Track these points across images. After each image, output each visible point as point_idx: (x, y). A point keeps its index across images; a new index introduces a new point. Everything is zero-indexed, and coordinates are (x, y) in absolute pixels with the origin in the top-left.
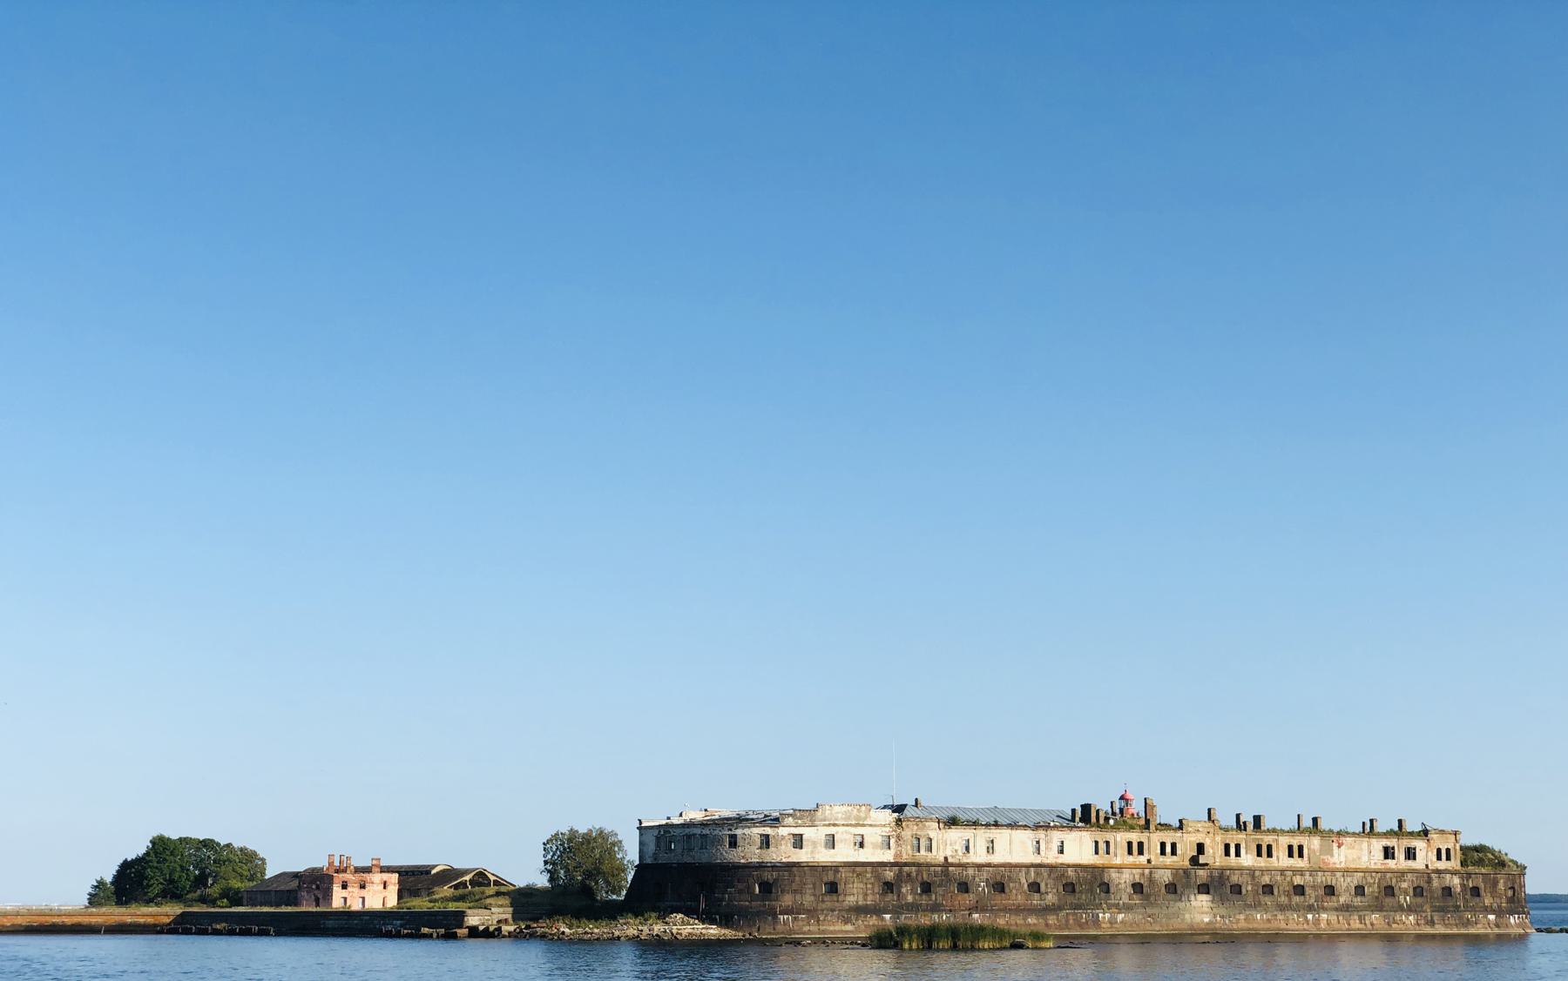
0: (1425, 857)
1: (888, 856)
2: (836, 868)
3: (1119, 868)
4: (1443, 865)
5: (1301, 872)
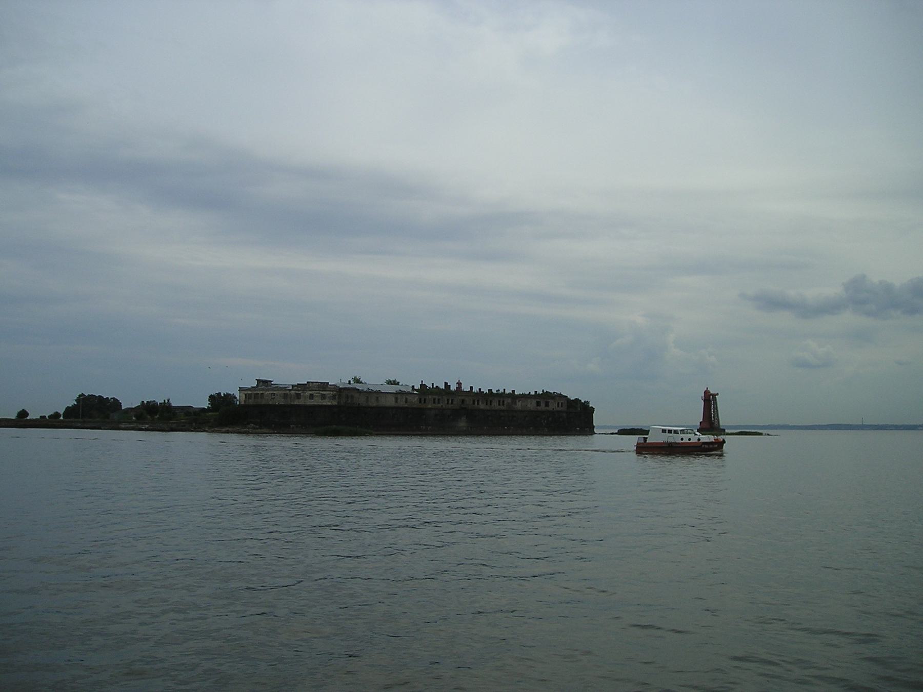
0: (553, 406)
1: (335, 403)
2: (314, 406)
3: (430, 409)
4: (560, 409)
5: (503, 411)
